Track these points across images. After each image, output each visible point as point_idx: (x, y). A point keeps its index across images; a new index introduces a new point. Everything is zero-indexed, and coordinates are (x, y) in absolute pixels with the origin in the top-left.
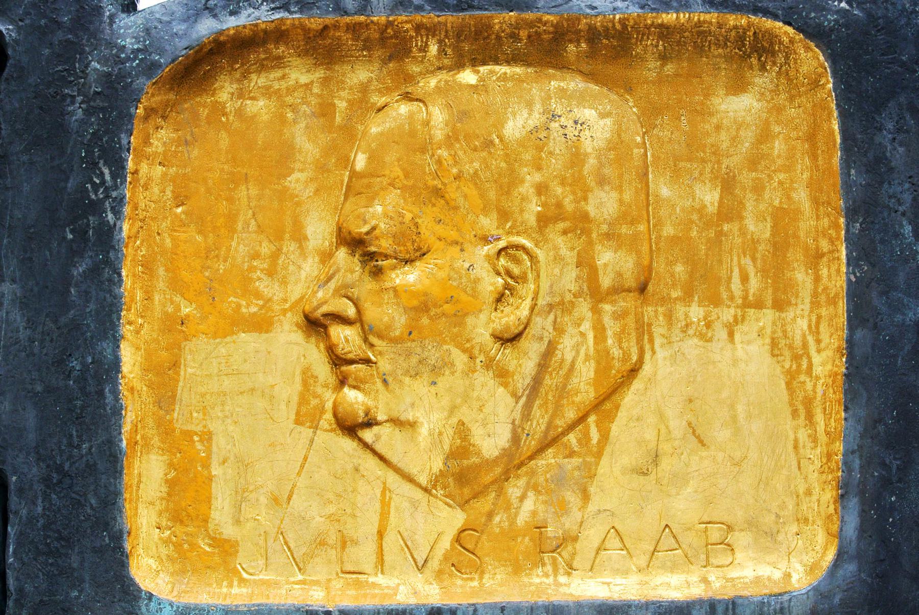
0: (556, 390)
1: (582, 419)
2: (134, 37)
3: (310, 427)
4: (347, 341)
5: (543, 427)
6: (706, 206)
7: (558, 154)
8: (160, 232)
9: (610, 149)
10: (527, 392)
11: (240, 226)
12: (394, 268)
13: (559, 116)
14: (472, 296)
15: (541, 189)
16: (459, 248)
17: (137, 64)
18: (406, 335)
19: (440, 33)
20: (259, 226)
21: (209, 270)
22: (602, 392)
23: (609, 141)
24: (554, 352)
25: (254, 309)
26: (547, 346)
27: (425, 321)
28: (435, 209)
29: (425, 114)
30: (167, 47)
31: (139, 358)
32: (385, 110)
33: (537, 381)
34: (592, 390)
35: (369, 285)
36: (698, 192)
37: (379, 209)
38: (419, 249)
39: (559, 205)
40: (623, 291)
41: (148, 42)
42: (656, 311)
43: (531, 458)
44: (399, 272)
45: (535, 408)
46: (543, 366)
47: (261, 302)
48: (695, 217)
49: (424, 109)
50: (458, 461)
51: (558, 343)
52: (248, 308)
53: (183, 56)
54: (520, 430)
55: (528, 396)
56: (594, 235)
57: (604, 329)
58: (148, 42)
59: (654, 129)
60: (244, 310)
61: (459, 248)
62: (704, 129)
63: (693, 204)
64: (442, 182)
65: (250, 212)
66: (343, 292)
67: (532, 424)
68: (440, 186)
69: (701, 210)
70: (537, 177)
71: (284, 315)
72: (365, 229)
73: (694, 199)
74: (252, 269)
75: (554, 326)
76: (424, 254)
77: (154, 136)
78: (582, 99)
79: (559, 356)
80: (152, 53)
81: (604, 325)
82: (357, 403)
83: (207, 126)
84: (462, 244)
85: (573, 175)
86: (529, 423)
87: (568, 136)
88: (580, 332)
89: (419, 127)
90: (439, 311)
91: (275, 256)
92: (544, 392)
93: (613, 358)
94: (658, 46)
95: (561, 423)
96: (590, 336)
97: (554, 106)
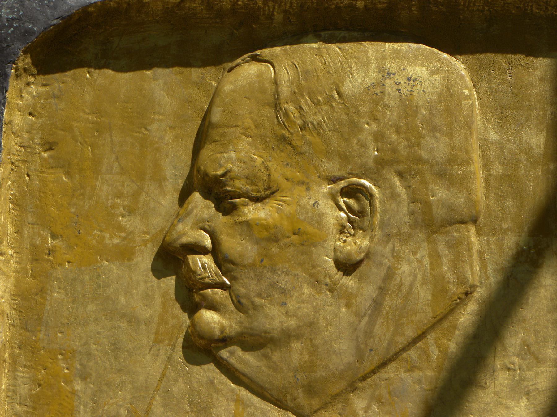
0: (396, 310)
1: (420, 337)
2: (9, 8)
3: (169, 345)
4: (204, 267)
5: (385, 344)
6: (532, 148)
7: (393, 107)
8: (30, 173)
9: (440, 102)
10: (369, 312)
11: (104, 169)
12: (245, 205)
13: (394, 74)
14: (318, 228)
15: (379, 137)
16: (305, 187)
17: (12, 31)
18: (258, 262)
19: (285, 4)
20: (122, 169)
21: (75, 207)
22: (438, 313)
23: (440, 95)
24: (393, 277)
25: (116, 241)
26: (387, 272)
27: (275, 249)
28: (282, 154)
29: (273, 73)
30: (40, 17)
31: (9, 285)
32: (235, 70)
33: (377, 304)
34: (429, 309)
35: (220, 220)
36: (524, 135)
37: (233, 154)
38: (269, 188)
39: (394, 150)
40: (456, 223)
41: (22, 12)
42: (488, 240)
43: (374, 372)
44: (251, 208)
45: (377, 326)
46: (382, 290)
47: (123, 234)
48: (522, 157)
49: (272, 69)
50: (306, 374)
51: (396, 269)
52: (111, 240)
53: (54, 25)
54: (363, 346)
55: (370, 315)
56: (427, 176)
57: (439, 257)
58: (22, 12)
59: (482, 81)
60: (107, 241)
61: (305, 187)
62: (529, 81)
63: (520, 146)
64: (289, 132)
65: (114, 156)
66: (201, 224)
67: (374, 341)
68: (287, 135)
69: (528, 151)
70: (374, 127)
71: (146, 246)
72: (220, 172)
73: (521, 142)
74: (114, 206)
75: (393, 254)
76: (274, 193)
77: (257, 181)
78: (415, 59)
79: (398, 279)
80: (25, 22)
81: (439, 253)
82: (214, 322)
83: (73, 82)
84: (307, 184)
85: (407, 124)
86: (372, 339)
87: (402, 91)
88: (416, 259)
89: (267, 85)
90: (287, 241)
91: (136, 195)
92: (384, 311)
93: (449, 282)
94: (484, 11)
95: (402, 341)
96: (426, 261)
97: (389, 65)
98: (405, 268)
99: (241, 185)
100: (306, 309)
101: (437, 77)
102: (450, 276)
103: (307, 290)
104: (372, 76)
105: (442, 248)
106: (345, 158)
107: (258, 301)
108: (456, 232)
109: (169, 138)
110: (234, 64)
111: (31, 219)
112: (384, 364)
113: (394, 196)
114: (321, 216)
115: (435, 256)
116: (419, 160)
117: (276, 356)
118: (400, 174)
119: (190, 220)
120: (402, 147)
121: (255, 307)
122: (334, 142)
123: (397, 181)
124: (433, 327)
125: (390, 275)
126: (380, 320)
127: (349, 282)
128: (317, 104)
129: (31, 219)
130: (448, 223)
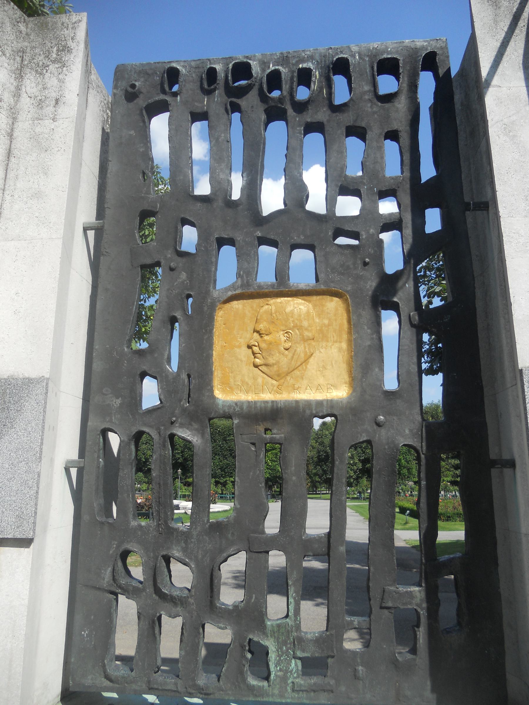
1: (301, 364)
15: (293, 321)
33: (293, 357)
39: (297, 324)
46: (294, 354)
57: (306, 347)
95: (297, 365)
96: (303, 348)
98: (298, 349)
99: (263, 332)
100: (277, 359)
101: (306, 308)
102: (308, 351)
103: (277, 354)
104: (292, 308)
105: (306, 345)
106: (286, 326)
107: (267, 357)
108: (309, 342)
109: (249, 322)
110: (424, 440)
111: (221, 339)
112: (293, 370)
113: (296, 334)
114: (280, 339)
115: (305, 347)
116: (301, 326)
117: (271, 368)
118: (298, 329)
119: (253, 340)
120: (298, 324)
121: (267, 359)
122: (284, 323)
123: (297, 331)
124: (304, 362)
125: (295, 351)
126: (293, 361)
127: (286, 352)
128: (280, 314)
129: (221, 339)
130: (308, 340)
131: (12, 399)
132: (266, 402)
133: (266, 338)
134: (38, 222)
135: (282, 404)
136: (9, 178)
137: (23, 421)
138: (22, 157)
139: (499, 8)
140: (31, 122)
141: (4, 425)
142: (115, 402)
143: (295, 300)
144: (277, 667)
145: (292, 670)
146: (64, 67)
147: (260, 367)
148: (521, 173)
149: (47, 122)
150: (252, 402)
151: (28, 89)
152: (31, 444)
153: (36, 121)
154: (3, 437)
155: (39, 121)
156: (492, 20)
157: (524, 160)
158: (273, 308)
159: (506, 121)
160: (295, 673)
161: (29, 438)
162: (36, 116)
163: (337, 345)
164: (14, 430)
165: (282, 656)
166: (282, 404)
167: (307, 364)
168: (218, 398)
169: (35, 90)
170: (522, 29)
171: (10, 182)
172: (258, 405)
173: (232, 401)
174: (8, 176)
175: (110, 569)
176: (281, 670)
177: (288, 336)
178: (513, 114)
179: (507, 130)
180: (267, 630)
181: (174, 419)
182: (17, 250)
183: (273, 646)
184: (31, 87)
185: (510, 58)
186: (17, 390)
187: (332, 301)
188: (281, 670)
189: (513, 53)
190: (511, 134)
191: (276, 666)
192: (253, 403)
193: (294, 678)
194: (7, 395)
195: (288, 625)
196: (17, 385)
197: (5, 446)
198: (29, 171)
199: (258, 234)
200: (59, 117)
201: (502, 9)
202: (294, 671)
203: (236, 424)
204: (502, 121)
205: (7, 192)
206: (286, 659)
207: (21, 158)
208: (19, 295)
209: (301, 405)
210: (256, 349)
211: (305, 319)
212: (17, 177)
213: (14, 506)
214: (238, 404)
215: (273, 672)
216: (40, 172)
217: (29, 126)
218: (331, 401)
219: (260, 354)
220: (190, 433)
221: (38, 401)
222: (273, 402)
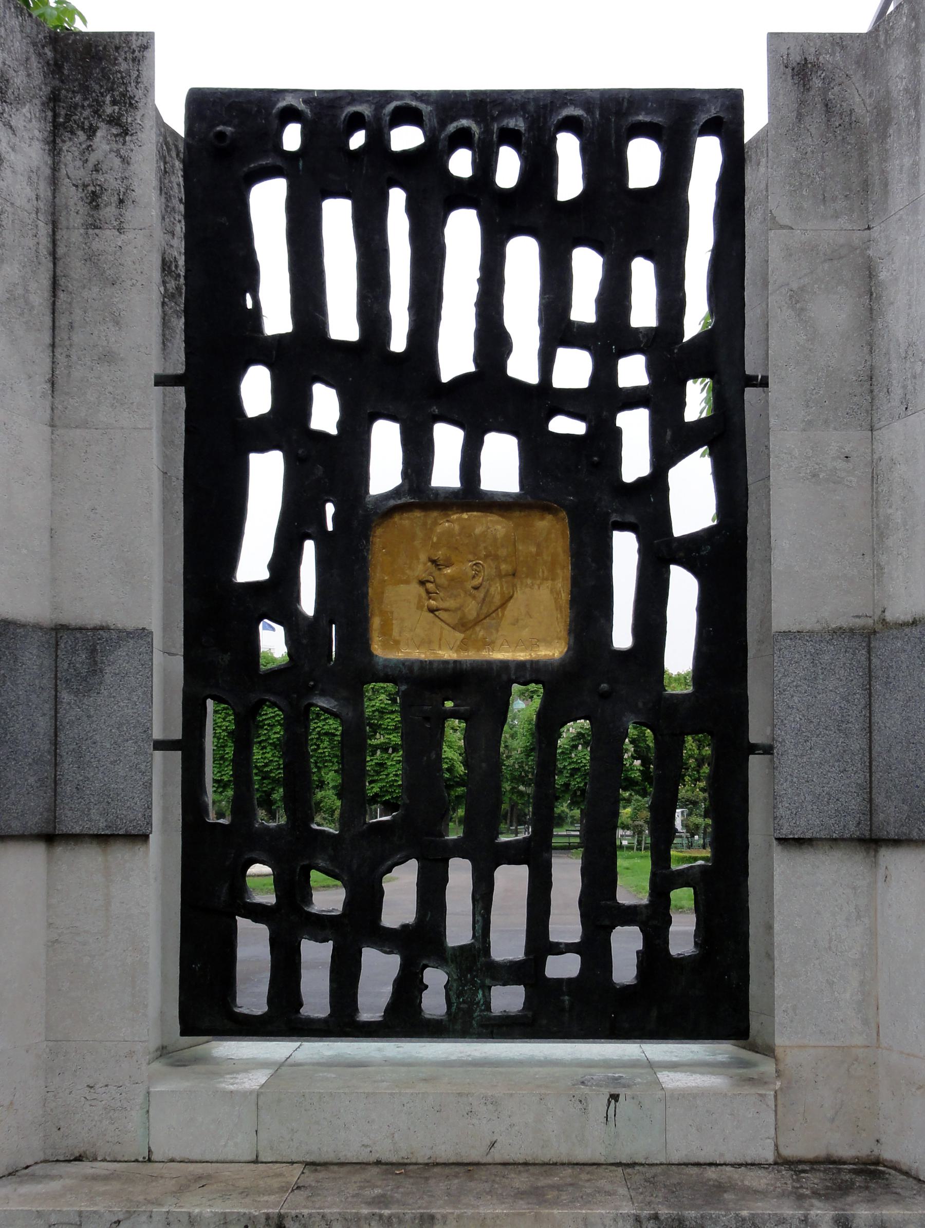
15: (485, 548)
95: (491, 611)
99: (441, 562)
106: (475, 554)
131: (106, 659)
132: (446, 662)
133: (448, 571)
134: (113, 402)
135: (468, 665)
136: (59, 327)
137: (125, 688)
138: (75, 292)
139: (808, 90)
140: (82, 231)
141: (98, 693)
142: (222, 659)
143: (489, 516)
144: (459, 999)
145: (479, 1002)
146: (127, 134)
147: (437, 613)
148: (805, 366)
149: (109, 233)
150: (426, 661)
151: (70, 169)
152: (139, 718)
153: (90, 231)
154: (98, 708)
155: (97, 231)
156: (795, 112)
157: (812, 347)
158: (457, 527)
159: (795, 286)
160: (482, 1005)
161: (135, 711)
162: (90, 221)
163: (549, 583)
164: (113, 699)
165: (466, 985)
166: (468, 665)
167: (505, 609)
168: (377, 656)
169: (81, 173)
170: (836, 130)
171: (62, 335)
172: (435, 665)
173: (398, 660)
174: (57, 324)
175: (227, 885)
176: (464, 1002)
177: (478, 570)
178: (805, 275)
179: (794, 299)
180: (447, 954)
181: (312, 683)
182: (86, 443)
183: (455, 973)
184: (75, 167)
185: (812, 182)
186: (111, 646)
187: (542, 519)
188: (464, 1002)
189: (817, 173)
190: (798, 306)
191: (458, 997)
192: (428, 663)
193: (481, 1011)
194: (97, 654)
195: (475, 947)
196: (111, 639)
197: (103, 721)
198: (90, 316)
199: (434, 411)
200: (128, 227)
201: (812, 93)
202: (482, 1002)
203: (403, 691)
204: (788, 284)
205: (58, 351)
206: (471, 989)
207: (74, 294)
208: (97, 511)
209: (495, 668)
210: (430, 586)
211: (502, 546)
212: (71, 326)
213: (122, 795)
214: (406, 664)
215: (454, 1003)
216: (107, 319)
217: (81, 239)
218: (537, 662)
219: (437, 593)
220: (336, 703)
221: (143, 662)
222: (455, 662)
